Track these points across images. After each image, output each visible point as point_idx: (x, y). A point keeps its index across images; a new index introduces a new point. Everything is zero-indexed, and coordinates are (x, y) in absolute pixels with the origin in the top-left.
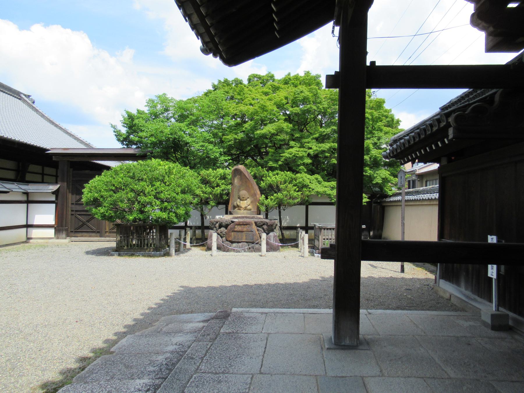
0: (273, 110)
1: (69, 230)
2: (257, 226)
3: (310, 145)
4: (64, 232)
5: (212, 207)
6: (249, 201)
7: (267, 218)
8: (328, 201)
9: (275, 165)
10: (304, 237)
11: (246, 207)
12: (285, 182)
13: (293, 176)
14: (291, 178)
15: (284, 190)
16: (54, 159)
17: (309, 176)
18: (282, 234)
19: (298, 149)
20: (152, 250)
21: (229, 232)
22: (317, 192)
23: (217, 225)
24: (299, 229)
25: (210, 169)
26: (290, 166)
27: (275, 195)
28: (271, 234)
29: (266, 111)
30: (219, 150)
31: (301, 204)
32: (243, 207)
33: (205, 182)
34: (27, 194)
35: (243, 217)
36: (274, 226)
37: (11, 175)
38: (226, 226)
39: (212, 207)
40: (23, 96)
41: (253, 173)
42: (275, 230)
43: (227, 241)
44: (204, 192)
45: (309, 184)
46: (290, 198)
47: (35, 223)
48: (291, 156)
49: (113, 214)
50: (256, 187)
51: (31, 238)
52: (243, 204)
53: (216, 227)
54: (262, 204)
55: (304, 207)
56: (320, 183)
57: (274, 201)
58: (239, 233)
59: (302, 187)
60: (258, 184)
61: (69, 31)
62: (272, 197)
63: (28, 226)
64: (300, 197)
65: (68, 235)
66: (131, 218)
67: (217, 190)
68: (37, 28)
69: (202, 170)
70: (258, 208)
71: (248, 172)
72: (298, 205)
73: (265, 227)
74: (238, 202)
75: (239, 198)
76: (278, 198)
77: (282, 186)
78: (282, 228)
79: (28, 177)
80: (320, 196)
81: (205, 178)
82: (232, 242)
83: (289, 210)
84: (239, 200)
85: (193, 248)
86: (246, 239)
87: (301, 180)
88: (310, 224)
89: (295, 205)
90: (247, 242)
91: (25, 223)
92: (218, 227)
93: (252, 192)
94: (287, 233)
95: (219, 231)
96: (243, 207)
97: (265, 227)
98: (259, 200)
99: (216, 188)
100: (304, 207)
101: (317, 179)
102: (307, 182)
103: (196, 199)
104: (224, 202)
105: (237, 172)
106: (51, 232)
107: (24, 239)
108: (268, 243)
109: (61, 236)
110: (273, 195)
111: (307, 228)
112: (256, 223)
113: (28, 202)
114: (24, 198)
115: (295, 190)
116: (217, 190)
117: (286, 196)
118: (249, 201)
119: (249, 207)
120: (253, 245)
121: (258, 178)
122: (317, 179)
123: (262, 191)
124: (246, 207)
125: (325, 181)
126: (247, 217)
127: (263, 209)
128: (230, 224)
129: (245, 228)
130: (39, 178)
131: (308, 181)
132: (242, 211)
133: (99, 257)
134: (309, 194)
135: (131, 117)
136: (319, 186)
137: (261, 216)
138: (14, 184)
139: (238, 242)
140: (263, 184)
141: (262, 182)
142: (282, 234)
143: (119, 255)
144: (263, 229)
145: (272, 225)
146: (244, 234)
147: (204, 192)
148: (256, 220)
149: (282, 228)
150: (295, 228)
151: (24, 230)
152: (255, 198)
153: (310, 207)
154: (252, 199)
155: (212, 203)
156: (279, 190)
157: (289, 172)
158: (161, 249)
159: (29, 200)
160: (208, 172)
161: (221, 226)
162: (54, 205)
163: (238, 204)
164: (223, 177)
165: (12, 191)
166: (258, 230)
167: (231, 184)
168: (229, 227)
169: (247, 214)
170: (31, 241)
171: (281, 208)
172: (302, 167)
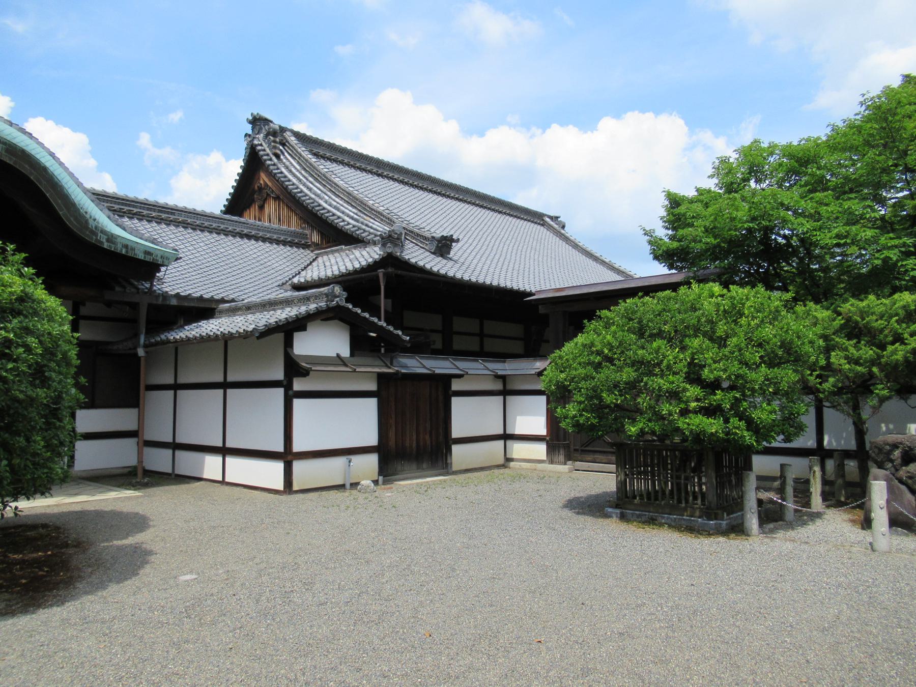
1: (572, 447)
4: (562, 452)
5: (882, 400)
16: (542, 310)
20: (697, 513)
23: (897, 453)
25: (872, 297)
30: (896, 242)
33: (854, 330)
34: (503, 378)
37: (518, 347)
39: (882, 400)
40: (548, 220)
47: (518, 432)
49: (595, 421)
51: (512, 460)
53: (892, 461)
61: (650, 115)
63: (507, 437)
65: (569, 458)
66: (633, 429)
67: (895, 352)
68: (607, 124)
69: (846, 301)
79: (458, 343)
81: (857, 323)
85: (827, 511)
91: (501, 432)
92: (899, 461)
95: (903, 473)
99: (890, 348)
106: (540, 450)
107: (501, 460)
109: (556, 459)
113: (505, 393)
114: (498, 386)
116: (895, 352)
130: (473, 344)
133: (582, 518)
135: (674, 201)
138: (477, 361)
143: (623, 517)
147: (850, 360)
151: (501, 443)
155: (881, 390)
158: (718, 513)
159: (507, 390)
160: (863, 304)
162: (372, 403)
165: (467, 373)
170: (512, 464)
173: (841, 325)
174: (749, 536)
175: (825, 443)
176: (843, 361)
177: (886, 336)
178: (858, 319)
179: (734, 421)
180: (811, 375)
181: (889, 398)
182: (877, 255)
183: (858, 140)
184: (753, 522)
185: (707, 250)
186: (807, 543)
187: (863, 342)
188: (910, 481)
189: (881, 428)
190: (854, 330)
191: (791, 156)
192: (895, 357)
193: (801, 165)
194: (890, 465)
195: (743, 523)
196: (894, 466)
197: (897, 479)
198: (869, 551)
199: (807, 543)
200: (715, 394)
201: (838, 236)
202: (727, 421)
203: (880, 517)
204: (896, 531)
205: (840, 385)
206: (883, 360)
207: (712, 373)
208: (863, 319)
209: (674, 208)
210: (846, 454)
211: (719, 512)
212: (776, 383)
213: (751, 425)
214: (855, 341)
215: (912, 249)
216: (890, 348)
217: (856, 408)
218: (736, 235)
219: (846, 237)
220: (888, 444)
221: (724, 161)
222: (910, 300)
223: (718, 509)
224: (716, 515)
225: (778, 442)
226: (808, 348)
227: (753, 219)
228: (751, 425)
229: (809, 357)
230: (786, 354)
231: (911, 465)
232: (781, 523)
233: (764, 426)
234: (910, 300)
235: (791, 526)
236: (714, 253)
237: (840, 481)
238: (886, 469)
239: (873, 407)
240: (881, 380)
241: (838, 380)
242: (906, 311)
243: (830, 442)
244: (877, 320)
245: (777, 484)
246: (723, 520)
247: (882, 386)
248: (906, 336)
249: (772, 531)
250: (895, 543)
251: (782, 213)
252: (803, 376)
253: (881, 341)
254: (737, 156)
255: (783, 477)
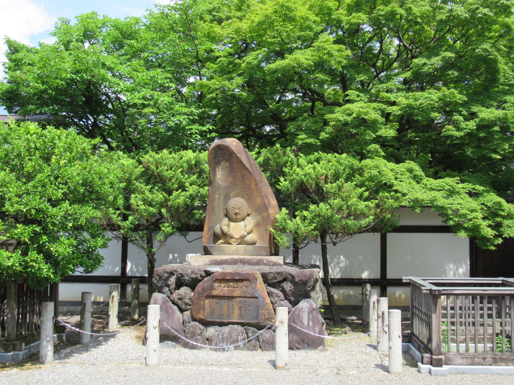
0: (307, 19)
2: (269, 285)
3: (392, 97)
5: (167, 236)
6: (250, 222)
7: (295, 262)
8: (438, 222)
9: (311, 140)
10: (378, 305)
11: (242, 238)
12: (336, 177)
13: (356, 163)
14: (351, 168)
15: (335, 195)
17: (392, 165)
18: (330, 297)
19: (364, 105)
21: (198, 299)
22: (416, 201)
23: (173, 280)
24: (368, 286)
26: (346, 140)
27: (312, 207)
28: (304, 304)
29: (292, 20)
31: (373, 229)
32: (237, 236)
33: (151, 178)
35: (235, 262)
36: (311, 283)
38: (193, 284)
39: (167, 236)
41: (261, 159)
42: (312, 294)
43: (194, 320)
44: (145, 201)
45: (395, 183)
46: (349, 215)
48: (349, 119)
50: (269, 191)
52: (237, 229)
53: (168, 286)
54: (283, 230)
55: (378, 235)
56: (417, 179)
57: (311, 222)
58: (224, 302)
59: (379, 187)
60: (274, 183)
62: (305, 213)
64: (372, 212)
69: (147, 152)
70: (272, 240)
71: (251, 158)
72: (367, 231)
73: (288, 286)
74: (224, 225)
75: (226, 216)
76: (319, 216)
77: (329, 186)
78: (328, 283)
80: (418, 210)
82: (207, 324)
83: (347, 243)
84: (226, 220)
85: (122, 330)
86: (241, 316)
87: (375, 172)
88: (391, 275)
89: (361, 231)
90: (242, 324)
92: (173, 286)
93: (258, 200)
94: (339, 294)
95: (175, 296)
96: (237, 235)
97: (288, 286)
98: (276, 220)
100: (378, 235)
101: (411, 171)
102: (389, 177)
103: (130, 218)
104: (189, 222)
105: (222, 154)
108: (292, 330)
110: (307, 209)
111: (383, 284)
112: (264, 276)
115: (360, 197)
116: (178, 197)
117: (340, 210)
118: (250, 222)
119: (250, 238)
120: (256, 330)
121: (275, 172)
122: (411, 171)
123: (283, 199)
124: (243, 237)
125: (427, 176)
126: (244, 262)
127: (284, 241)
128: (203, 278)
129: (238, 290)
131: (391, 176)
132: (234, 247)
134: (396, 204)
136: (417, 186)
137: (279, 259)
139: (222, 324)
140: (284, 184)
141: (282, 179)
142: (330, 297)
144: (283, 291)
145: (305, 283)
146: (235, 303)
147: (145, 201)
148: (266, 269)
149: (328, 283)
150: (360, 283)
152: (265, 214)
153: (390, 237)
154: (259, 218)
155: (166, 227)
156: (321, 196)
157: (344, 155)
160: (157, 156)
161: (179, 284)
163: (225, 229)
164: (193, 168)
166: (270, 294)
167: (210, 184)
168: (199, 287)
169: (246, 253)
171: (328, 239)
172: (374, 147)
173: (142, 172)
174: (43, 363)
175: (128, 269)
176: (140, 203)
177: (173, 184)
178: (154, 168)
179: (33, 255)
180: (115, 213)
181: (171, 234)
182: (172, 118)
183: (165, 23)
184: (48, 349)
185: (35, 94)
186: (94, 364)
187: (156, 188)
188: (180, 302)
189: (169, 256)
190: (151, 178)
191: (116, 27)
192: (178, 201)
193: (124, 38)
194: (167, 289)
195: (38, 352)
196: (170, 290)
197: (171, 301)
198: (143, 366)
199: (94, 364)
200: (16, 228)
201: (144, 98)
202: (25, 254)
203: (153, 334)
204: (167, 344)
205: (137, 223)
206: (169, 203)
207: (13, 206)
208: (157, 168)
209: (13, 53)
210: (142, 280)
211: (18, 343)
212: (76, 219)
213: (48, 257)
214: (150, 186)
215: (196, 117)
216: (175, 193)
217: (150, 241)
218: (62, 85)
219: (150, 100)
220: (166, 272)
221: (66, 22)
222: (192, 157)
223: (17, 339)
224: (14, 345)
225: (80, 271)
226: (107, 188)
227: (77, 72)
228: (48, 257)
229: (109, 196)
230: (87, 193)
231: (182, 288)
232: (78, 346)
233: (63, 259)
234: (192, 157)
235: (86, 348)
236: (41, 99)
237: (136, 301)
238: (163, 293)
239: (160, 242)
240: (167, 219)
241: (135, 218)
242: (189, 165)
243: (131, 268)
244: (167, 170)
245: (79, 308)
246: (20, 351)
247: (168, 224)
248: (187, 184)
249: (67, 356)
250: (164, 355)
251: (103, 71)
252: (107, 214)
253: (169, 187)
254: (77, 22)
255: (82, 303)
